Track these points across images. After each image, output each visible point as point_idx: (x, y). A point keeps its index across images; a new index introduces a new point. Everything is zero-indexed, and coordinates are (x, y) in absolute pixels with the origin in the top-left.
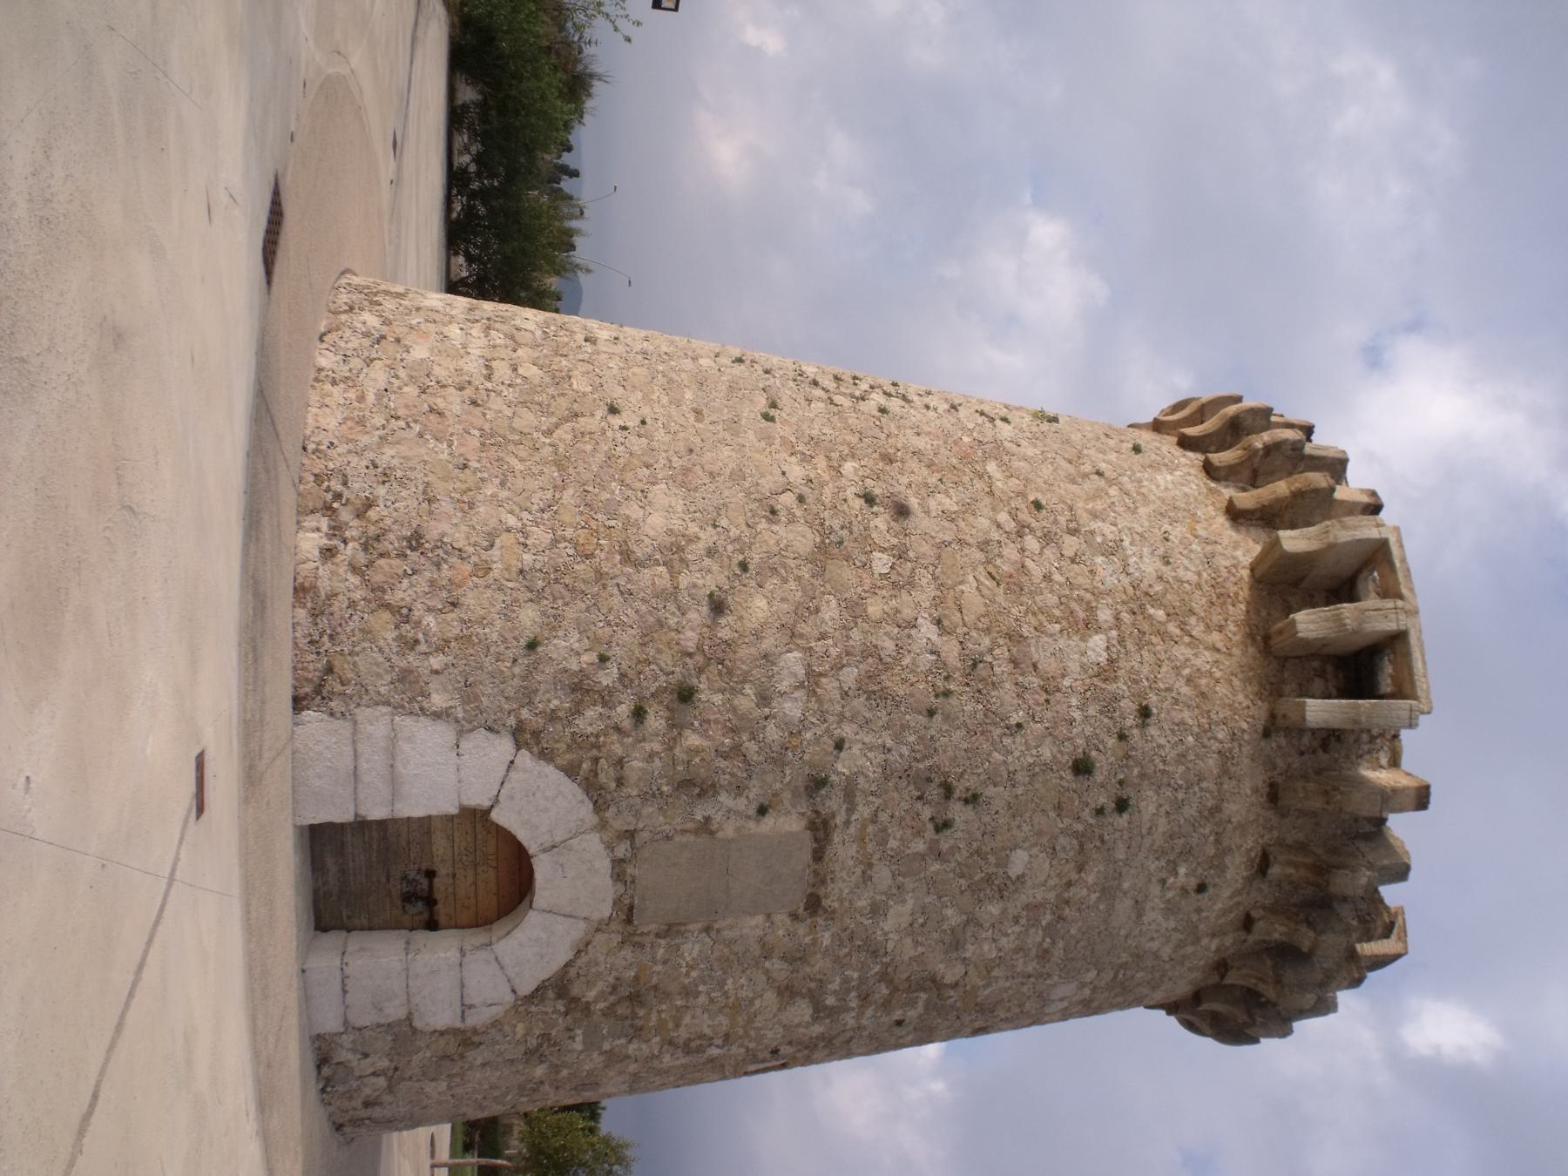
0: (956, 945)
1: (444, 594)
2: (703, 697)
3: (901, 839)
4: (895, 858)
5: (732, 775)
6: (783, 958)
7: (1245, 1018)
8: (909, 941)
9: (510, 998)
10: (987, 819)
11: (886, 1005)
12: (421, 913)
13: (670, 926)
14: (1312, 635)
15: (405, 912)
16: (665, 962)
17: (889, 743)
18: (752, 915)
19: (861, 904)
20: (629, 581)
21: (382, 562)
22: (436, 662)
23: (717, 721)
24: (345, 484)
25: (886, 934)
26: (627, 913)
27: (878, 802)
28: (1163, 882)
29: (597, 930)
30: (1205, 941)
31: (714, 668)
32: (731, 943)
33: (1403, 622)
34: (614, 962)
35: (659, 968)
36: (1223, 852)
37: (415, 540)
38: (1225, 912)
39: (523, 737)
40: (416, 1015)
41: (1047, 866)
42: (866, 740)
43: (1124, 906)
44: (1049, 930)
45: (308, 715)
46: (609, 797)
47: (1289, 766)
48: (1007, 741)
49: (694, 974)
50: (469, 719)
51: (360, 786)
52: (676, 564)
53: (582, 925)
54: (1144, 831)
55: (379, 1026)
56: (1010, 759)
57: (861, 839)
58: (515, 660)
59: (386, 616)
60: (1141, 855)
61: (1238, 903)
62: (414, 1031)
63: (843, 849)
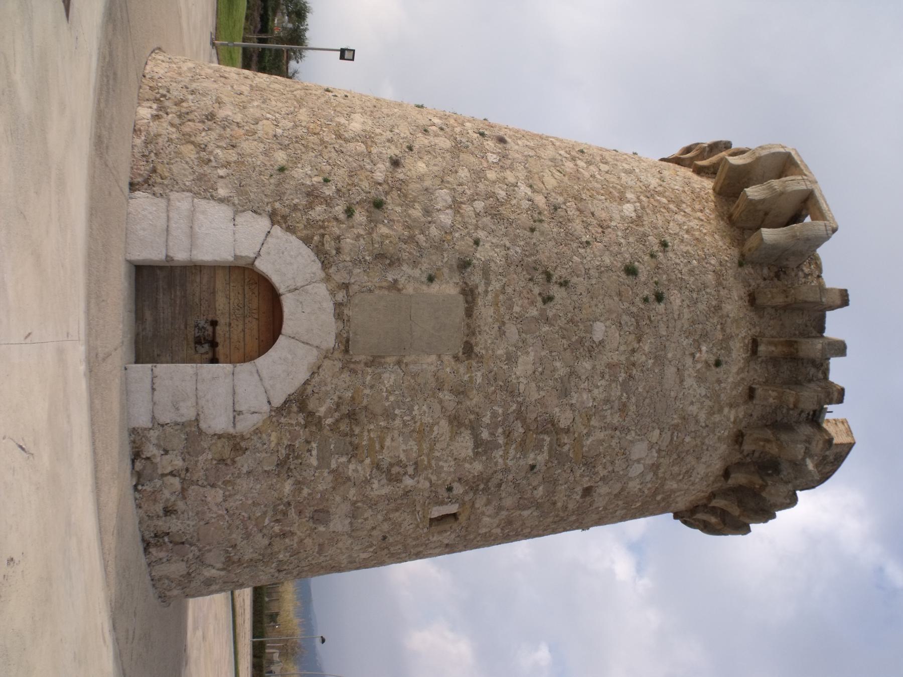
0: (566, 393)
1: (228, 141)
2: (390, 208)
3: (522, 306)
4: (519, 319)
5: (410, 253)
6: (451, 391)
7: (760, 482)
8: (533, 385)
9: (266, 408)
10: (575, 298)
11: (523, 446)
12: (207, 353)
13: (374, 357)
14: (757, 198)
15: (196, 351)
16: (372, 387)
17: (508, 244)
18: (429, 354)
19: (500, 352)
20: (341, 146)
21: (190, 123)
22: (222, 172)
23: (398, 221)
24: (168, 92)
25: (518, 378)
26: (345, 344)
27: (505, 280)
28: (693, 355)
29: (325, 357)
30: (726, 410)
31: (395, 193)
32: (415, 376)
33: (810, 186)
34: (337, 384)
35: (367, 391)
36: (728, 338)
37: (211, 117)
38: (736, 385)
39: (274, 218)
40: (202, 416)
41: (617, 335)
42: (494, 241)
43: (671, 371)
44: (624, 385)
45: (138, 194)
46: (331, 260)
47: (758, 285)
48: (582, 251)
49: (392, 398)
50: (242, 204)
51: (170, 237)
52: (369, 143)
53: (315, 352)
54: (676, 317)
55: (177, 424)
56: (585, 261)
57: (496, 304)
58: (271, 175)
59: (191, 147)
60: (677, 334)
61: (743, 379)
62: (201, 432)
63: (485, 311)
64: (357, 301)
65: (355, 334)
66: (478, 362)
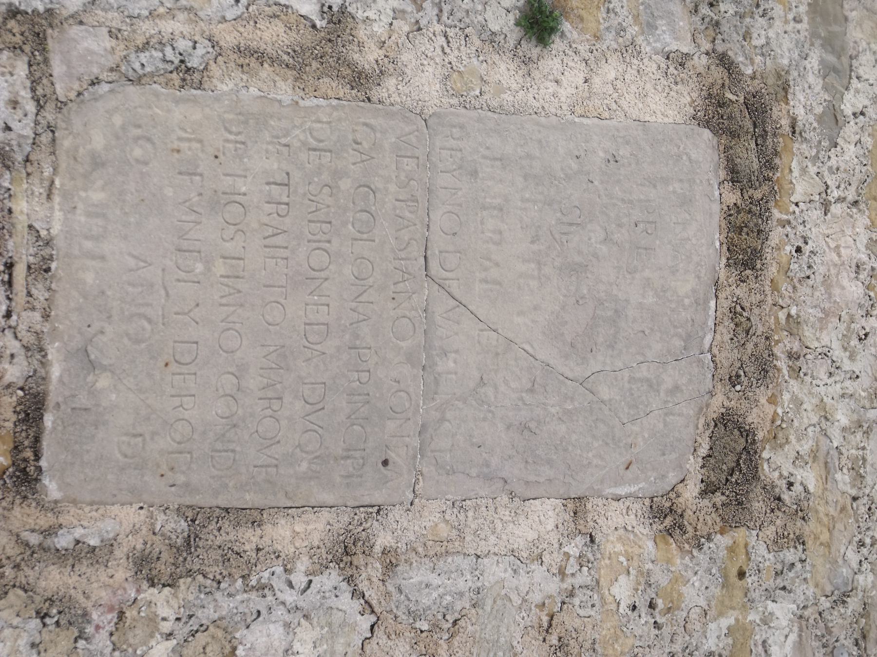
13: (197, 518)
18: (521, 498)
64: (98, 141)
65: (86, 360)
66: (778, 543)
